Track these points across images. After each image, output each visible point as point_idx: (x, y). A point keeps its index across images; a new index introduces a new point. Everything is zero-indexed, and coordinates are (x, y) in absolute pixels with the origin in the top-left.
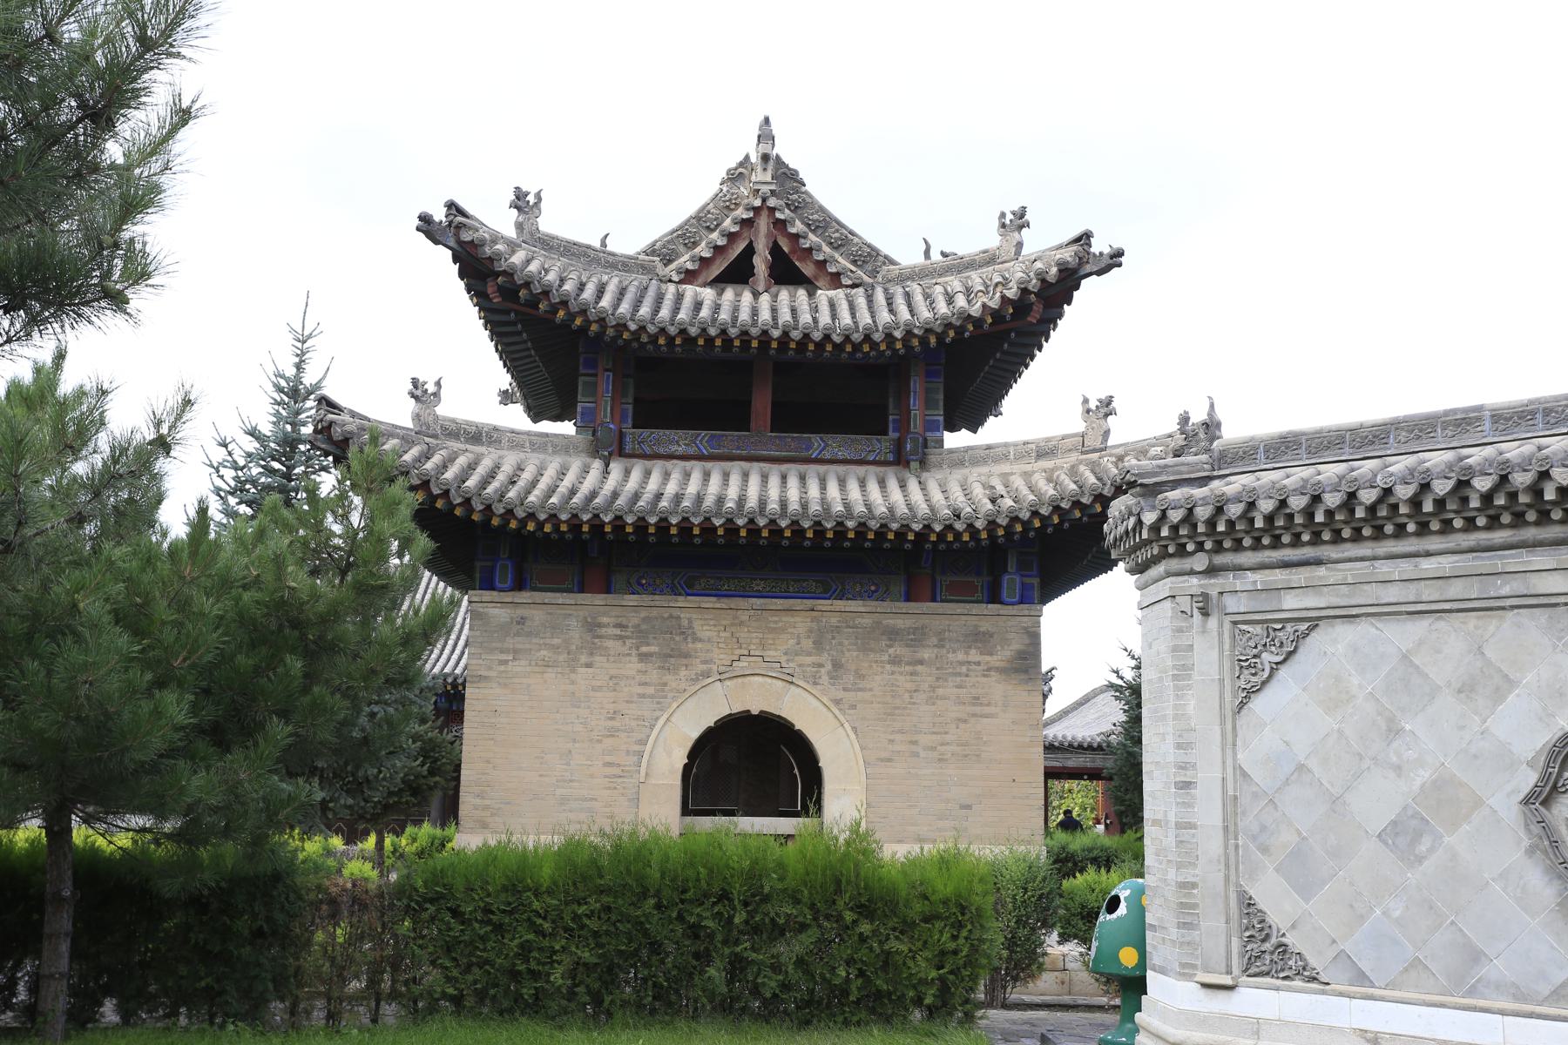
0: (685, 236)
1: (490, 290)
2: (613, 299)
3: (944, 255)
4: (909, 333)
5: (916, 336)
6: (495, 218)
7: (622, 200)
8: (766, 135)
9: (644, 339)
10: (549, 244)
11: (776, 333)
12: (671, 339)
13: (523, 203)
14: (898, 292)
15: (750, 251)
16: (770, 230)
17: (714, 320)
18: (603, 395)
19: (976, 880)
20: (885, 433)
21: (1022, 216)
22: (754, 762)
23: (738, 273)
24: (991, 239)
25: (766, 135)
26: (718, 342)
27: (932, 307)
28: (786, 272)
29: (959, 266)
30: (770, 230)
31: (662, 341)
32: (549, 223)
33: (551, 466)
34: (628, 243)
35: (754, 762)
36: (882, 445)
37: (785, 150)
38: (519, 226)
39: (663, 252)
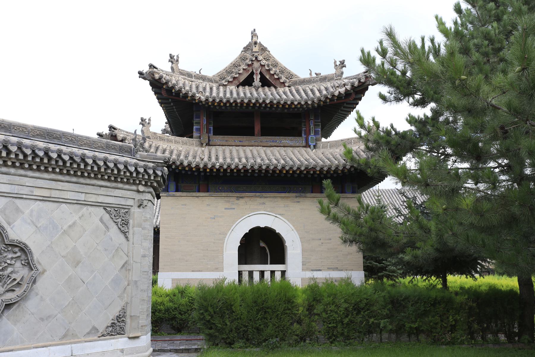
0: (228, 71)
1: (162, 92)
2: (205, 92)
3: (316, 74)
4: (221, 101)
5: (223, 102)
6: (164, 66)
7: (207, 60)
8: (254, 34)
9: (222, 104)
10: (182, 73)
11: (239, 101)
12: (231, 104)
13: (173, 60)
14: (293, 88)
15: (252, 73)
16: (256, 68)
17: (232, 97)
18: (201, 122)
19: (334, 281)
20: (301, 136)
21: (343, 64)
22: (262, 245)
23: (248, 82)
24: (330, 70)
25: (254, 34)
26: (234, 105)
27: (318, 92)
28: (265, 83)
29: (324, 79)
30: (256, 68)
31: (228, 105)
32: (182, 66)
33: (190, 151)
34: (211, 71)
35: (262, 245)
36: (301, 141)
37: (261, 40)
38: (172, 68)
39: (221, 76)
